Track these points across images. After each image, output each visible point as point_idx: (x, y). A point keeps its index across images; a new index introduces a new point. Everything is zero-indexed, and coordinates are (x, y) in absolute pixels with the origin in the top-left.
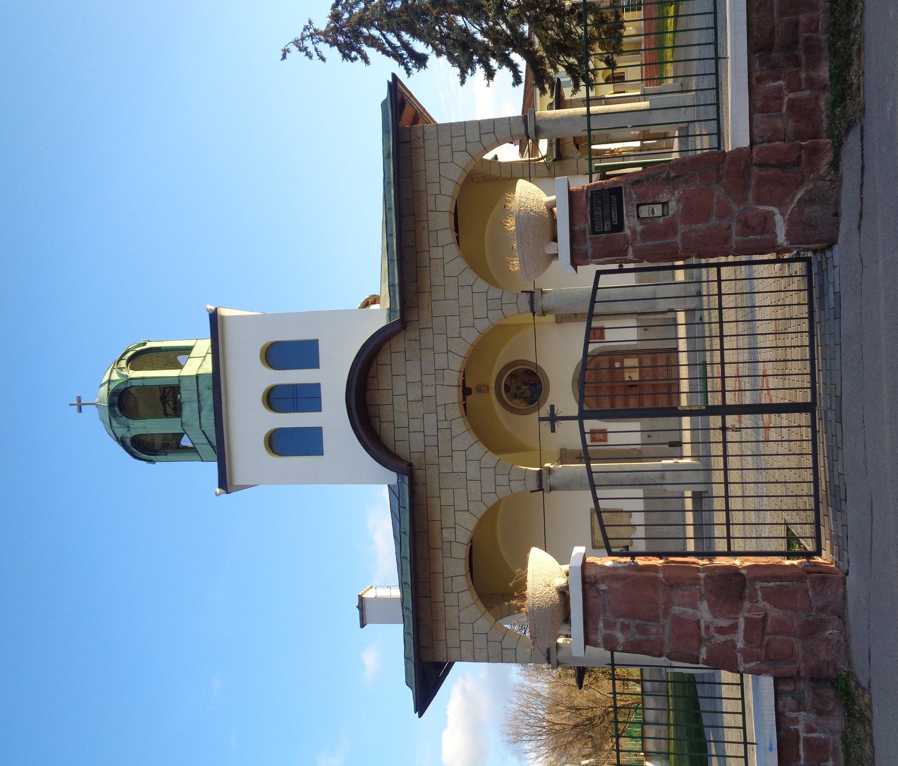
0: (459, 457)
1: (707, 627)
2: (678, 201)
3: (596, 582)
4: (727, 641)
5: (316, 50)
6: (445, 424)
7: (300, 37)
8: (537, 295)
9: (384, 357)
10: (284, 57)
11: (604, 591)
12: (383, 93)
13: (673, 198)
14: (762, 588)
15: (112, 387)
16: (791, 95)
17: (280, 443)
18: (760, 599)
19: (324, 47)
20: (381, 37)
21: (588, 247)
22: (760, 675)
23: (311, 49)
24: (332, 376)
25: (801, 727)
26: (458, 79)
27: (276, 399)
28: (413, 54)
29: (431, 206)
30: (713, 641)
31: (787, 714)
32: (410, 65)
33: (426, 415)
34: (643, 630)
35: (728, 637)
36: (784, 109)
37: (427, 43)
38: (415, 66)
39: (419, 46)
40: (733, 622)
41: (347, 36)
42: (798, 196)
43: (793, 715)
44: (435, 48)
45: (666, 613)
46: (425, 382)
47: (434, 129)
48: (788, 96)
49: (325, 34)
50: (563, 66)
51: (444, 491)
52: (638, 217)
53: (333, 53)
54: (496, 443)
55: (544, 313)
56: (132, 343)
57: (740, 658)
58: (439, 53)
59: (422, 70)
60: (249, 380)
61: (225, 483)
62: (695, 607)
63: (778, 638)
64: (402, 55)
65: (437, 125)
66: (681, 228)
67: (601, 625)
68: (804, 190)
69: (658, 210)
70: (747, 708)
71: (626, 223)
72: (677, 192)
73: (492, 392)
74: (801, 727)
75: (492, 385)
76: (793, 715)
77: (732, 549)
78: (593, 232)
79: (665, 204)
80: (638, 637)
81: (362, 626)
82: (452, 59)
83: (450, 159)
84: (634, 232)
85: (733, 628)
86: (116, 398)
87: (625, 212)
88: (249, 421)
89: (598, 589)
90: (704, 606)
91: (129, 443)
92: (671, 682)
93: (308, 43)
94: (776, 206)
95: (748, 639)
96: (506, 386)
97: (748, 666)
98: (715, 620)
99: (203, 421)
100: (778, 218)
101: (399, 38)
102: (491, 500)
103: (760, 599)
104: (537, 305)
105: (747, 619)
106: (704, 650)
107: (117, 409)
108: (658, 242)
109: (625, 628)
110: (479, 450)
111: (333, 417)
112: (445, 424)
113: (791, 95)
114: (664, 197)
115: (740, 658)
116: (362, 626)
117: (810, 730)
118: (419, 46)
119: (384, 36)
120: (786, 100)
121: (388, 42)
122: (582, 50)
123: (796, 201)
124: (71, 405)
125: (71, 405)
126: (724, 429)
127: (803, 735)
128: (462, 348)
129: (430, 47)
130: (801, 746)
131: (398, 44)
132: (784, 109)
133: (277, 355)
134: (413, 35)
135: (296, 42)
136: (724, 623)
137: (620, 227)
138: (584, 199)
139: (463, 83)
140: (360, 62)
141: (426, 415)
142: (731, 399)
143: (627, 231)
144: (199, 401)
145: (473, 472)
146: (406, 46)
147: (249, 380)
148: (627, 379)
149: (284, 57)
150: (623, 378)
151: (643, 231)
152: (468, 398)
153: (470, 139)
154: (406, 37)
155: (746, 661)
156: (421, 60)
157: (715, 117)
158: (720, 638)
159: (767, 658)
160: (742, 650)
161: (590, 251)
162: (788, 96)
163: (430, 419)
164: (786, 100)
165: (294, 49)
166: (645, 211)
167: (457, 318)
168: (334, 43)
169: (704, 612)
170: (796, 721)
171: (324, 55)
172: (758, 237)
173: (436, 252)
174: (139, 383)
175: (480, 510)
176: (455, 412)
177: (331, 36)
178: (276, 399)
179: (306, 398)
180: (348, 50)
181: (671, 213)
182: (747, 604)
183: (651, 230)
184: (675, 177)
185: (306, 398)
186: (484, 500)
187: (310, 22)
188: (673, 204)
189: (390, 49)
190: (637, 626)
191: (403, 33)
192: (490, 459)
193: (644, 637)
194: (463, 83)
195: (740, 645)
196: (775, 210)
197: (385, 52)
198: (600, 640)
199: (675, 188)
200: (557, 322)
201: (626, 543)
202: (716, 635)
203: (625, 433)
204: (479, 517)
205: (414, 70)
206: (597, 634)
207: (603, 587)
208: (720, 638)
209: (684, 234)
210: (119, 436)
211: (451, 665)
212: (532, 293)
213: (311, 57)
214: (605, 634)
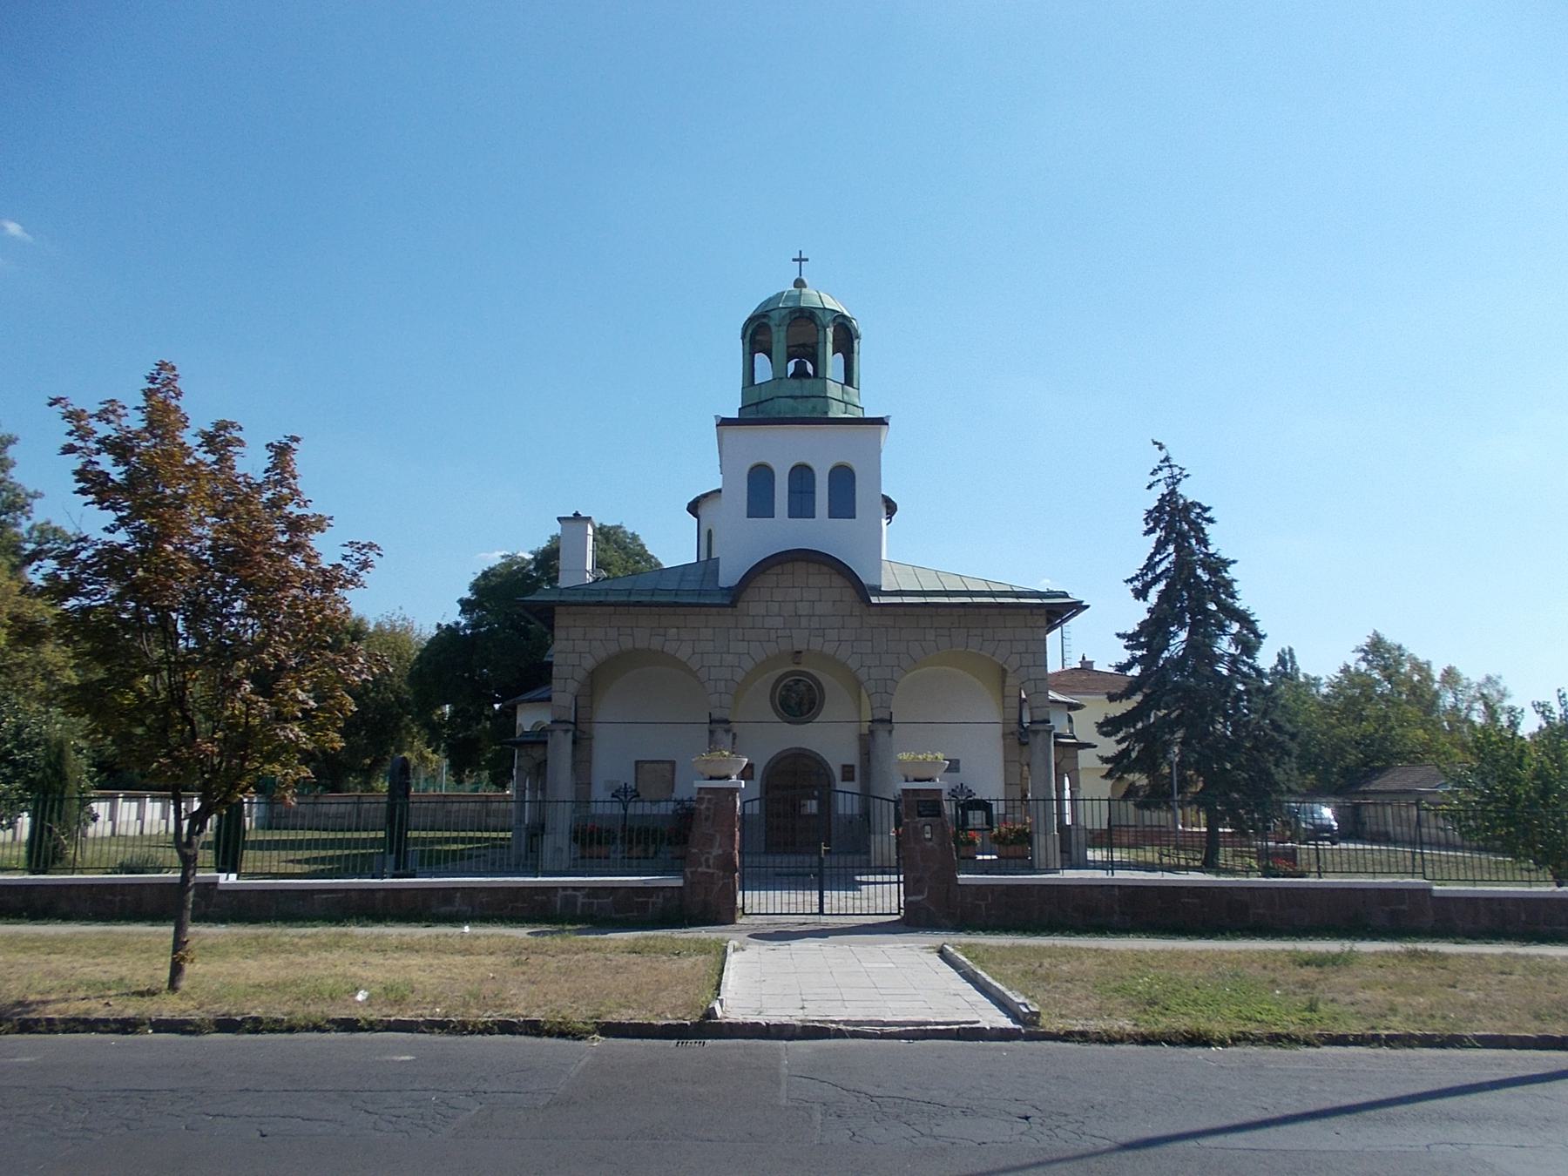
6: (773, 636)
8: (888, 727)
9: (838, 581)
15: (819, 313)
17: (760, 477)
19: (1162, 489)
23: (1161, 475)
26: (1122, 631)
27: (802, 505)
49: (1173, 493)
56: (860, 325)
61: (724, 422)
88: (783, 448)
92: (185, 879)
93: (1166, 473)
100: (920, 898)
104: (879, 726)
109: (708, 809)
112: (773, 636)
122: (1148, 763)
129: (1136, 613)
133: (843, 479)
139: (1118, 635)
146: (1156, 580)
156: (1141, 594)
165: (1162, 455)
166: (928, 828)
169: (716, 851)
179: (802, 475)
180: (1154, 517)
183: (918, 832)
185: (802, 475)
194: (1118, 635)
212: (890, 721)
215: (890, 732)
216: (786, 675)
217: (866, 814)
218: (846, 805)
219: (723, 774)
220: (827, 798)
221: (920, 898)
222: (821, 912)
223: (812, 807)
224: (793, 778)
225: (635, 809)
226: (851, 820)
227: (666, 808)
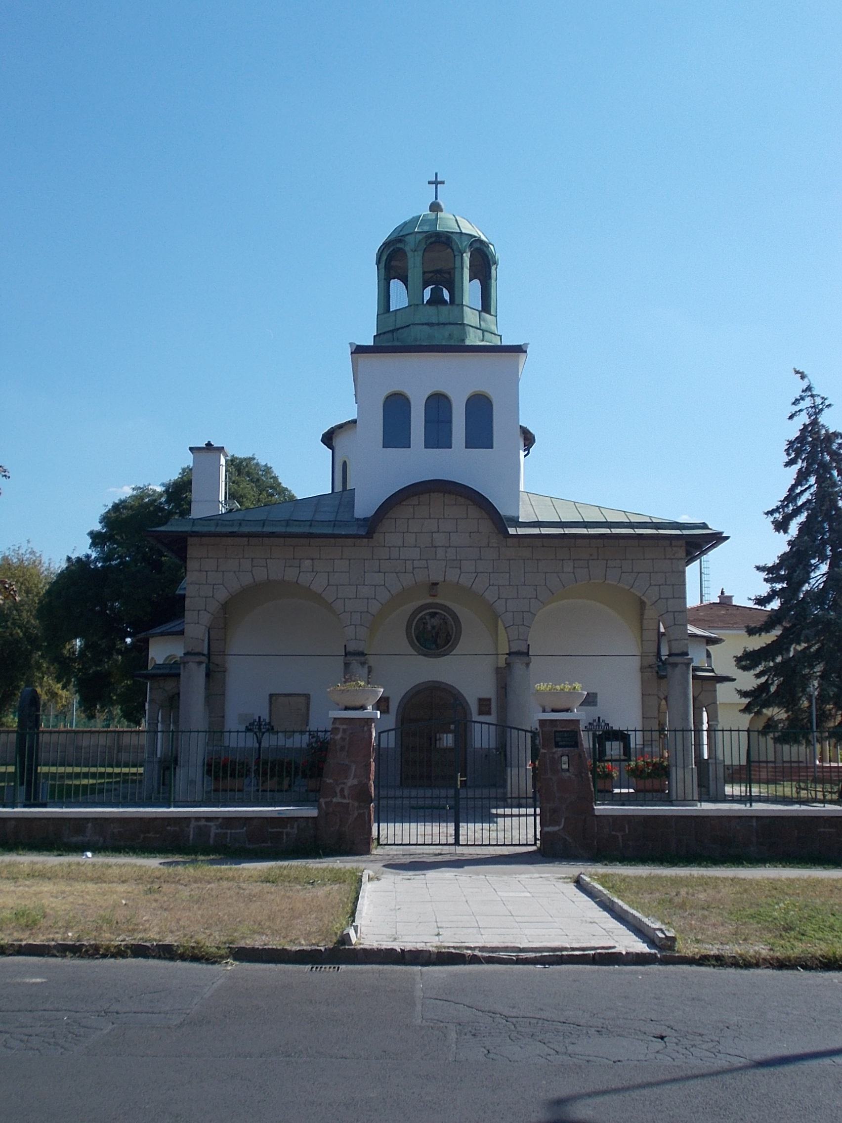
1: (344, 783)
5: (800, 411)
6: (409, 568)
7: (814, 393)
8: (525, 659)
10: (797, 372)
12: (715, 526)
16: (620, 838)
17: (396, 407)
19: (803, 419)
23: (803, 405)
24: (457, 462)
25: (288, 830)
26: (762, 564)
28: (788, 519)
32: (777, 515)
33: (418, 549)
34: (342, 748)
41: (813, 448)
43: (295, 826)
49: (814, 423)
50: (767, 680)
51: (348, 562)
53: (793, 430)
56: (498, 250)
60: (456, 378)
61: (359, 350)
67: (345, 727)
73: (430, 600)
74: (288, 830)
76: (295, 826)
78: (556, 731)
79: (568, 770)
81: (191, 449)
82: (784, 558)
83: (653, 582)
84: (554, 753)
85: (344, 797)
86: (443, 239)
90: (355, 782)
91: (400, 245)
93: (808, 402)
96: (436, 613)
99: (420, 327)
100: (556, 828)
106: (331, 781)
107: (433, 239)
109: (343, 739)
111: (419, 462)
112: (409, 568)
113: (620, 838)
116: (191, 449)
117: (288, 834)
120: (618, 834)
121: (802, 492)
124: (436, 174)
125: (436, 174)
127: (285, 831)
130: (278, 830)
131: (800, 503)
133: (480, 409)
135: (809, 388)
136: (346, 793)
137: (557, 745)
139: (758, 568)
140: (786, 459)
141: (418, 549)
143: (555, 750)
144: (438, 324)
146: (797, 512)
147: (456, 378)
149: (797, 372)
153: (671, 602)
155: (326, 803)
156: (781, 526)
158: (338, 790)
164: (618, 834)
165: (804, 384)
166: (565, 759)
168: (804, 430)
169: (351, 782)
170: (292, 828)
171: (795, 418)
174: (458, 264)
177: (811, 429)
178: (438, 404)
180: (796, 448)
182: (356, 804)
183: (556, 762)
185: (438, 435)
187: (829, 405)
188: (568, 774)
189: (798, 491)
194: (758, 568)
195: (334, 800)
196: (562, 826)
197: (792, 489)
198: (337, 726)
199: (576, 776)
200: (497, 668)
204: (323, 595)
207: (366, 729)
208: (338, 790)
210: (408, 239)
212: (527, 654)
213: (794, 403)
215: (528, 665)
217: (502, 747)
218: (483, 736)
219: (358, 703)
221: (556, 828)
222: (457, 843)
227: (300, 741)
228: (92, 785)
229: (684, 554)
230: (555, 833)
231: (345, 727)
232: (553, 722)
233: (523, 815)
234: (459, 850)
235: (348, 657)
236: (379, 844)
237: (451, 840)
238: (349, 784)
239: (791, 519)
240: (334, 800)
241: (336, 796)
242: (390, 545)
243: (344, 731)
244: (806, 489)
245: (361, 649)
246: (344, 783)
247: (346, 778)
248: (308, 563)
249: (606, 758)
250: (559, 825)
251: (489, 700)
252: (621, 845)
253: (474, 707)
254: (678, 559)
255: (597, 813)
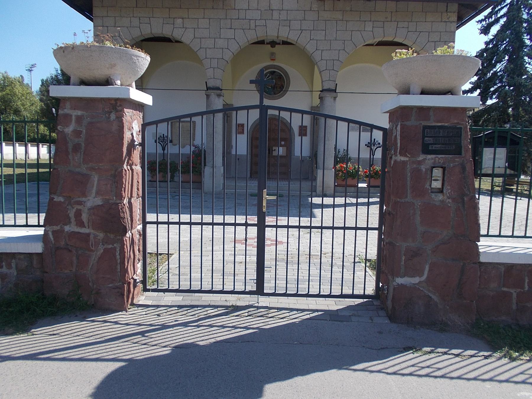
0: (230, 34)
1: (80, 203)
2: (442, 201)
3: (117, 111)
4: (69, 219)
6: (253, 26)
8: (334, 94)
11: (109, 118)
13: (445, 197)
14: (115, 249)
18: (105, 247)
20: (505, 4)
21: (413, 122)
22: (43, 242)
29: (401, 25)
30: (70, 207)
31: (13, 261)
32: (484, 23)
33: (259, 12)
34: (76, 148)
35: (73, 220)
36: (505, 289)
37: (495, 36)
38: (483, 26)
39: (495, 30)
40: (86, 225)
42: (433, 297)
43: (13, 265)
44: (491, 41)
45: (92, 169)
46: (282, 12)
47: (453, 29)
48: (514, 292)
51: (208, 21)
52: (434, 167)
54: (240, 58)
55: (321, 98)
57: (56, 228)
58: (487, 43)
59: (479, 31)
62: (98, 193)
63: (74, 258)
64: (492, 18)
65: (455, 32)
66: (418, 203)
67: (79, 113)
68: (438, 301)
69: (437, 185)
70: (16, 230)
71: (430, 156)
72: (450, 201)
73: (271, 63)
75: (275, 63)
76: (13, 265)
77: (148, 225)
78: (425, 127)
79: (441, 191)
80: (70, 146)
83: (430, 39)
84: (420, 163)
85: (81, 224)
87: (440, 156)
89: (111, 112)
90: (98, 201)
94: (428, 277)
95: (73, 234)
96: (274, 72)
97: (50, 233)
98: (86, 210)
100: (416, 280)
101: (501, 17)
102: (201, 54)
103: (106, 246)
105: (88, 235)
106: (61, 199)
108: (408, 183)
109: (77, 133)
110: (235, 48)
112: (253, 26)
113: (515, 295)
114: (447, 190)
115: (56, 228)
118: (495, 30)
119: (507, 5)
120: (512, 291)
121: (502, 8)
123: (430, 294)
126: (246, 225)
128: (303, 40)
129: (492, 37)
131: (499, 16)
132: (505, 289)
134: (503, 27)
136: (85, 217)
137: (426, 150)
138: (456, 121)
141: (259, 12)
142: (269, 233)
143: (421, 157)
145: (221, 43)
146: (497, 21)
148: (274, 148)
150: (274, 146)
151: (419, 171)
152: (269, 46)
154: (502, 21)
156: (485, 31)
157: (502, 234)
158: (72, 214)
159: (57, 249)
160: (62, 231)
161: (408, 123)
162: (514, 292)
163: (256, 15)
164: (512, 291)
166: (437, 173)
167: (323, 38)
169: (93, 200)
170: (9, 266)
172: (403, 263)
173: (369, 26)
175: (195, 47)
176: (261, 35)
181: (433, 195)
182: (101, 235)
183: (421, 178)
184: (463, 200)
186: (201, 50)
188: (440, 197)
189: (497, 9)
190: (79, 145)
191: (505, 19)
192: (228, 56)
193: (70, 150)
195: (67, 228)
199: (453, 200)
200: (312, 107)
201: (175, 141)
202: (74, 210)
203: (241, 145)
205: (479, 26)
206: (71, 108)
207: (113, 116)
209: (413, 203)
211: (91, 20)
212: (335, 91)
214: (71, 116)
215: (335, 98)
216: (266, 68)
217: (314, 155)
218: (301, 147)
219: (99, 73)
220: (289, 143)
221: (416, 280)
222: (260, 291)
223: (281, 151)
224: (270, 133)
225: (172, 150)
226: (302, 160)
227: (187, 150)
228: (18, 175)
229: (456, 19)
230: (413, 288)
231: (79, 113)
232: (423, 111)
233: (328, 206)
234: (264, 301)
235: (209, 91)
236: (145, 290)
237: (252, 286)
238: (89, 204)
239: (492, 26)
240: (67, 228)
241: (70, 222)
242: (239, 8)
243: (79, 119)
244: (505, 6)
245: (218, 85)
246: (80, 203)
247: (84, 195)
248: (179, 21)
249: (483, 172)
250: (421, 275)
251: (243, 124)
252: (514, 307)
253: (296, 130)
254: (451, 22)
255: (482, 259)
